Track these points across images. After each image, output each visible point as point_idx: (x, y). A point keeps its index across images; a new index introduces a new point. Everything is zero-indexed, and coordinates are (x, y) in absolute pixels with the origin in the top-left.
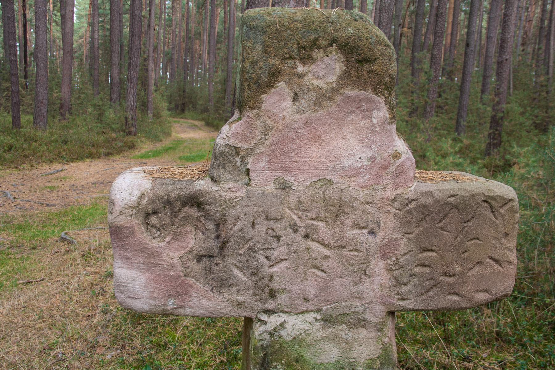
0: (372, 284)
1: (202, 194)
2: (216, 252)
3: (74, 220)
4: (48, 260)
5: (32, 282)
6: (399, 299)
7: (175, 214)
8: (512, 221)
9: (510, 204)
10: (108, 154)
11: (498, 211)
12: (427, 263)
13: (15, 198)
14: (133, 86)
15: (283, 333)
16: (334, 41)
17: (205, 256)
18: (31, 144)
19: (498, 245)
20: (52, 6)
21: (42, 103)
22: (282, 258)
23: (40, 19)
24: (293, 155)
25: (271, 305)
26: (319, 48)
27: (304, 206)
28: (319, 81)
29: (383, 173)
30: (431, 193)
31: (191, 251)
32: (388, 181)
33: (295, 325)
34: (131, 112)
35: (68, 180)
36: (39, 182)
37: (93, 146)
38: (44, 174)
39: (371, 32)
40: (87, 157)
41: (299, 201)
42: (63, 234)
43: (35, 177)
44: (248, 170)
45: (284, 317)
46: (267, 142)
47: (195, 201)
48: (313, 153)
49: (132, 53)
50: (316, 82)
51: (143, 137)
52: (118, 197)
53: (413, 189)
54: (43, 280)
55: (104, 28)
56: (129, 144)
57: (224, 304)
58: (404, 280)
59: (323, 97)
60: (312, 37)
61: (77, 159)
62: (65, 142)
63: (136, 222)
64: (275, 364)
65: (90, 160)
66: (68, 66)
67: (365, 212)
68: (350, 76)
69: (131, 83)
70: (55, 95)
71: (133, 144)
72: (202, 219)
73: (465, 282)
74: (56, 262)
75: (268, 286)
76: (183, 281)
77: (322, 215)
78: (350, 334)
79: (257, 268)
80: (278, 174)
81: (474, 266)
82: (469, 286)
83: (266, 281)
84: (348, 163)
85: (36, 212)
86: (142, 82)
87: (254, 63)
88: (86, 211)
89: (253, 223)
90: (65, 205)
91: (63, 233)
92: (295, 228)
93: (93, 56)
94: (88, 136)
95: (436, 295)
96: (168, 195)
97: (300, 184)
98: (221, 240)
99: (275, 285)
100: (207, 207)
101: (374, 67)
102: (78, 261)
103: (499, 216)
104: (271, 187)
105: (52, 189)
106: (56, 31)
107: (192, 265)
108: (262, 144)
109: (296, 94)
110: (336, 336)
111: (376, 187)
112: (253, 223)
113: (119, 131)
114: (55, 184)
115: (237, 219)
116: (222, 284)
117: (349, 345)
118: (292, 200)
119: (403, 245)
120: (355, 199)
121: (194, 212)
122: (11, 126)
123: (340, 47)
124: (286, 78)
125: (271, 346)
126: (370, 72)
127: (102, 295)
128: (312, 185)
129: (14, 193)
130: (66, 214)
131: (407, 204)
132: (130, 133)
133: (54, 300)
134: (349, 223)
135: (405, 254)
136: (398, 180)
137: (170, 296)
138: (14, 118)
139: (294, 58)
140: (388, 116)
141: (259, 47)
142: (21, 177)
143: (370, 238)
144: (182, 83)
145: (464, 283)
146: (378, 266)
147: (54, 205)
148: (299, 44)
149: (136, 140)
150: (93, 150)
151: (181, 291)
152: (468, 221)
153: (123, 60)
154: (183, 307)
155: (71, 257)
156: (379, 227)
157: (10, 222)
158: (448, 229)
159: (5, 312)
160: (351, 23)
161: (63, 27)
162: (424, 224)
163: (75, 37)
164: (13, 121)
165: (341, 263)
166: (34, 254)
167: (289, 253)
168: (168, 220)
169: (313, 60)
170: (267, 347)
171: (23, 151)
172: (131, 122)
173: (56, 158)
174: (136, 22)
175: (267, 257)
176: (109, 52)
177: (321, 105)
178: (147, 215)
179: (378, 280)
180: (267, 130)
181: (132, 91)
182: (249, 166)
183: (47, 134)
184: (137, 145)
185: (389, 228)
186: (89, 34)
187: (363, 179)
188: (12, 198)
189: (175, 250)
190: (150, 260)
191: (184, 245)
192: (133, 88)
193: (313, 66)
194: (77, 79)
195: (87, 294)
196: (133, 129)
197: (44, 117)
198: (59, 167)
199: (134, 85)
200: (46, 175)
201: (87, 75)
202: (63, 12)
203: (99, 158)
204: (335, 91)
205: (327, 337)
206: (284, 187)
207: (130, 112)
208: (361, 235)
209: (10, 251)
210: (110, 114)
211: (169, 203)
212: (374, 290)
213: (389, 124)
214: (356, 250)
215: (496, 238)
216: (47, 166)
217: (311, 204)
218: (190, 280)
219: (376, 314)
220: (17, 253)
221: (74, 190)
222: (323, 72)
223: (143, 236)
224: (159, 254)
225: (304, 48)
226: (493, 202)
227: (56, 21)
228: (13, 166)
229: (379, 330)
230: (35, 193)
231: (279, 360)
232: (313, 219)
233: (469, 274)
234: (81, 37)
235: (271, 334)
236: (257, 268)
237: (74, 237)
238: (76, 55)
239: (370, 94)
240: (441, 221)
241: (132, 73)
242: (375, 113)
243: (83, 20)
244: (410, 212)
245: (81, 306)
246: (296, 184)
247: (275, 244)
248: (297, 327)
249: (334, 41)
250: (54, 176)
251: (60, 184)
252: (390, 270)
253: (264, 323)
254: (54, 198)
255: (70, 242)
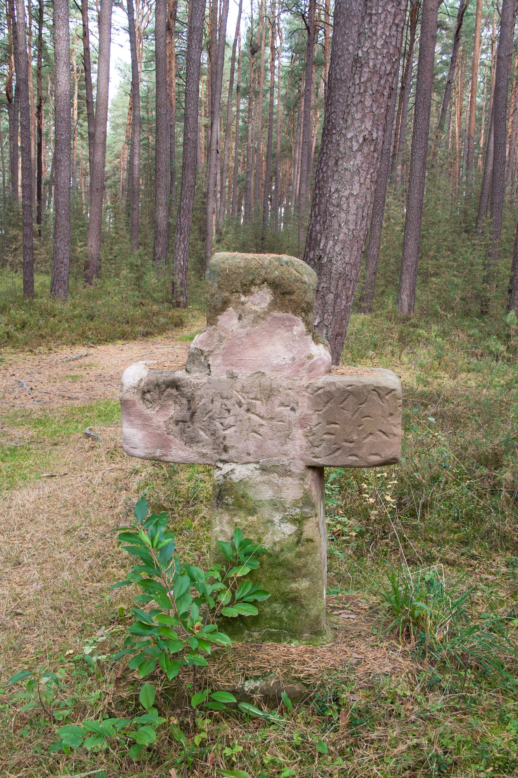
0: (294, 445)
1: (179, 380)
2: (188, 419)
3: (100, 416)
4: (71, 455)
5: (55, 476)
6: (314, 457)
7: (162, 393)
8: (394, 405)
9: (393, 393)
10: (146, 335)
11: (384, 397)
12: (332, 432)
13: (31, 389)
14: (184, 239)
15: (233, 476)
16: (265, 281)
17: (181, 421)
18: (49, 320)
19: (385, 422)
20: (76, 112)
21: (62, 263)
22: (232, 424)
23: (62, 150)
24: (239, 355)
25: (225, 457)
26: (255, 285)
27: (246, 390)
28: (256, 307)
29: (300, 369)
30: (334, 383)
31: (171, 418)
32: (304, 375)
33: (241, 472)
34: (180, 276)
35: (94, 368)
36: (59, 370)
37: (128, 322)
38: (64, 360)
39: (292, 273)
40: (119, 338)
41: (243, 387)
42: (87, 430)
43: (53, 363)
44: (209, 365)
45: (233, 466)
46: (222, 347)
47: (174, 384)
48: (252, 355)
49: (183, 192)
50: (253, 308)
51: (197, 310)
52: (126, 381)
53: (322, 380)
54: (66, 474)
55: (146, 146)
56: (175, 321)
57: (193, 455)
58: (316, 444)
59: (258, 318)
60: (251, 278)
61: (106, 341)
62: (91, 318)
63: (137, 398)
64: (227, 497)
65: (123, 342)
66: (97, 210)
67: (287, 395)
68: (276, 304)
69: (181, 234)
70: (79, 250)
71: (181, 320)
72: (179, 396)
73: (362, 447)
74: (79, 458)
75: (222, 443)
76: (166, 438)
77: (258, 396)
78: (280, 481)
79: (215, 431)
80: (229, 368)
81: (368, 436)
82: (364, 450)
83: (221, 439)
84: (275, 362)
85: (56, 406)
86: (200, 228)
87: (213, 295)
88: (114, 406)
89: (212, 400)
90: (90, 398)
91: (87, 429)
92: (240, 404)
93: (132, 192)
94: (121, 309)
95: (340, 455)
96: (157, 380)
97: (244, 375)
98: (191, 411)
99: (227, 443)
100: (182, 389)
101: (293, 297)
102: (103, 458)
103: (385, 401)
104: (224, 377)
105: (74, 379)
106: (80, 148)
107: (172, 426)
108: (218, 348)
109: (240, 315)
110: (270, 481)
111: (295, 378)
112: (212, 400)
113: (163, 302)
114: (78, 373)
115: (202, 397)
116: (192, 441)
117: (279, 489)
118: (238, 386)
119: (315, 419)
120: (281, 386)
121: (174, 392)
122: (20, 294)
123: (269, 284)
124: (234, 305)
125: (225, 484)
126: (290, 300)
127: (126, 490)
128: (252, 375)
129: (30, 383)
130: (90, 409)
131: (317, 391)
132: (178, 305)
133: (77, 492)
134: (277, 402)
135: (317, 425)
136: (311, 374)
137: (157, 447)
138: (25, 282)
139: (239, 292)
140: (305, 330)
141: (216, 285)
142: (36, 363)
143: (292, 413)
144: (260, 228)
145: (360, 448)
146: (298, 433)
147: (77, 398)
148: (242, 283)
149: (185, 314)
150: (127, 328)
151: (165, 444)
152: (362, 404)
153: (174, 194)
154: (166, 455)
155: (96, 454)
156: (297, 405)
157: (28, 416)
158: (347, 409)
159: (31, 500)
160: (278, 267)
161: (92, 150)
162: (329, 404)
163: (109, 157)
164: (25, 287)
165: (272, 429)
166: (56, 450)
167: (236, 421)
168: (157, 397)
169: (252, 294)
170: (221, 485)
171: (39, 329)
172: (179, 289)
173: (79, 339)
174: (189, 150)
175: (221, 424)
176: (154, 184)
177: (257, 323)
178: (144, 393)
179: (298, 442)
180: (221, 339)
181: (182, 246)
182: (210, 363)
183: (68, 307)
184: (186, 320)
185: (305, 407)
186: (127, 152)
187: (287, 372)
188: (28, 389)
189: (162, 416)
190: (145, 422)
191: (167, 413)
192: (184, 241)
193: (251, 297)
194: (108, 219)
195: (111, 489)
196: (182, 299)
197: (65, 283)
198: (81, 350)
199: (184, 236)
200: (67, 361)
201: (123, 216)
202: (92, 130)
203: (135, 339)
204: (266, 313)
205: (264, 482)
206: (233, 376)
207: (178, 275)
208: (286, 411)
209: (31, 446)
210: (152, 279)
211: (158, 385)
212: (295, 450)
213: (306, 335)
214: (282, 421)
215: (383, 416)
216: (69, 350)
217: (251, 388)
218: (171, 437)
219: (298, 467)
220: (38, 449)
221: (101, 381)
222: (259, 301)
223: (141, 406)
224: (151, 419)
225: (245, 285)
226: (380, 391)
227: (80, 134)
228: (27, 349)
229: (302, 479)
230: (54, 384)
231: (230, 495)
232: (252, 399)
233: (364, 441)
234: (117, 157)
235: (224, 477)
236: (215, 431)
237: (99, 433)
238: (109, 182)
239: (290, 315)
240: (342, 403)
241: (182, 220)
242: (295, 328)
243: (120, 131)
244: (319, 396)
245: (104, 498)
246: (240, 375)
247: (227, 415)
248: (242, 473)
249: (265, 281)
250: (76, 363)
251: (84, 373)
252: (307, 436)
253: (220, 469)
254: (77, 390)
255: (95, 439)
